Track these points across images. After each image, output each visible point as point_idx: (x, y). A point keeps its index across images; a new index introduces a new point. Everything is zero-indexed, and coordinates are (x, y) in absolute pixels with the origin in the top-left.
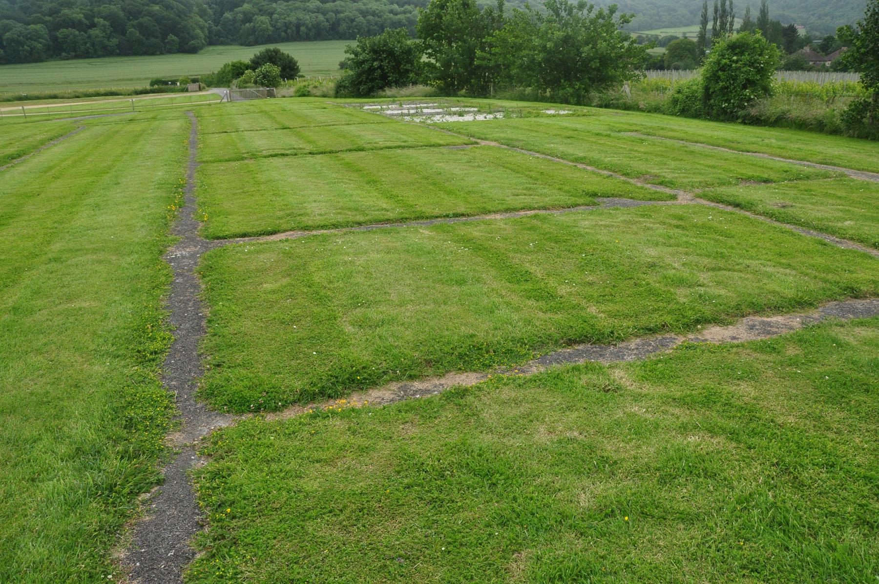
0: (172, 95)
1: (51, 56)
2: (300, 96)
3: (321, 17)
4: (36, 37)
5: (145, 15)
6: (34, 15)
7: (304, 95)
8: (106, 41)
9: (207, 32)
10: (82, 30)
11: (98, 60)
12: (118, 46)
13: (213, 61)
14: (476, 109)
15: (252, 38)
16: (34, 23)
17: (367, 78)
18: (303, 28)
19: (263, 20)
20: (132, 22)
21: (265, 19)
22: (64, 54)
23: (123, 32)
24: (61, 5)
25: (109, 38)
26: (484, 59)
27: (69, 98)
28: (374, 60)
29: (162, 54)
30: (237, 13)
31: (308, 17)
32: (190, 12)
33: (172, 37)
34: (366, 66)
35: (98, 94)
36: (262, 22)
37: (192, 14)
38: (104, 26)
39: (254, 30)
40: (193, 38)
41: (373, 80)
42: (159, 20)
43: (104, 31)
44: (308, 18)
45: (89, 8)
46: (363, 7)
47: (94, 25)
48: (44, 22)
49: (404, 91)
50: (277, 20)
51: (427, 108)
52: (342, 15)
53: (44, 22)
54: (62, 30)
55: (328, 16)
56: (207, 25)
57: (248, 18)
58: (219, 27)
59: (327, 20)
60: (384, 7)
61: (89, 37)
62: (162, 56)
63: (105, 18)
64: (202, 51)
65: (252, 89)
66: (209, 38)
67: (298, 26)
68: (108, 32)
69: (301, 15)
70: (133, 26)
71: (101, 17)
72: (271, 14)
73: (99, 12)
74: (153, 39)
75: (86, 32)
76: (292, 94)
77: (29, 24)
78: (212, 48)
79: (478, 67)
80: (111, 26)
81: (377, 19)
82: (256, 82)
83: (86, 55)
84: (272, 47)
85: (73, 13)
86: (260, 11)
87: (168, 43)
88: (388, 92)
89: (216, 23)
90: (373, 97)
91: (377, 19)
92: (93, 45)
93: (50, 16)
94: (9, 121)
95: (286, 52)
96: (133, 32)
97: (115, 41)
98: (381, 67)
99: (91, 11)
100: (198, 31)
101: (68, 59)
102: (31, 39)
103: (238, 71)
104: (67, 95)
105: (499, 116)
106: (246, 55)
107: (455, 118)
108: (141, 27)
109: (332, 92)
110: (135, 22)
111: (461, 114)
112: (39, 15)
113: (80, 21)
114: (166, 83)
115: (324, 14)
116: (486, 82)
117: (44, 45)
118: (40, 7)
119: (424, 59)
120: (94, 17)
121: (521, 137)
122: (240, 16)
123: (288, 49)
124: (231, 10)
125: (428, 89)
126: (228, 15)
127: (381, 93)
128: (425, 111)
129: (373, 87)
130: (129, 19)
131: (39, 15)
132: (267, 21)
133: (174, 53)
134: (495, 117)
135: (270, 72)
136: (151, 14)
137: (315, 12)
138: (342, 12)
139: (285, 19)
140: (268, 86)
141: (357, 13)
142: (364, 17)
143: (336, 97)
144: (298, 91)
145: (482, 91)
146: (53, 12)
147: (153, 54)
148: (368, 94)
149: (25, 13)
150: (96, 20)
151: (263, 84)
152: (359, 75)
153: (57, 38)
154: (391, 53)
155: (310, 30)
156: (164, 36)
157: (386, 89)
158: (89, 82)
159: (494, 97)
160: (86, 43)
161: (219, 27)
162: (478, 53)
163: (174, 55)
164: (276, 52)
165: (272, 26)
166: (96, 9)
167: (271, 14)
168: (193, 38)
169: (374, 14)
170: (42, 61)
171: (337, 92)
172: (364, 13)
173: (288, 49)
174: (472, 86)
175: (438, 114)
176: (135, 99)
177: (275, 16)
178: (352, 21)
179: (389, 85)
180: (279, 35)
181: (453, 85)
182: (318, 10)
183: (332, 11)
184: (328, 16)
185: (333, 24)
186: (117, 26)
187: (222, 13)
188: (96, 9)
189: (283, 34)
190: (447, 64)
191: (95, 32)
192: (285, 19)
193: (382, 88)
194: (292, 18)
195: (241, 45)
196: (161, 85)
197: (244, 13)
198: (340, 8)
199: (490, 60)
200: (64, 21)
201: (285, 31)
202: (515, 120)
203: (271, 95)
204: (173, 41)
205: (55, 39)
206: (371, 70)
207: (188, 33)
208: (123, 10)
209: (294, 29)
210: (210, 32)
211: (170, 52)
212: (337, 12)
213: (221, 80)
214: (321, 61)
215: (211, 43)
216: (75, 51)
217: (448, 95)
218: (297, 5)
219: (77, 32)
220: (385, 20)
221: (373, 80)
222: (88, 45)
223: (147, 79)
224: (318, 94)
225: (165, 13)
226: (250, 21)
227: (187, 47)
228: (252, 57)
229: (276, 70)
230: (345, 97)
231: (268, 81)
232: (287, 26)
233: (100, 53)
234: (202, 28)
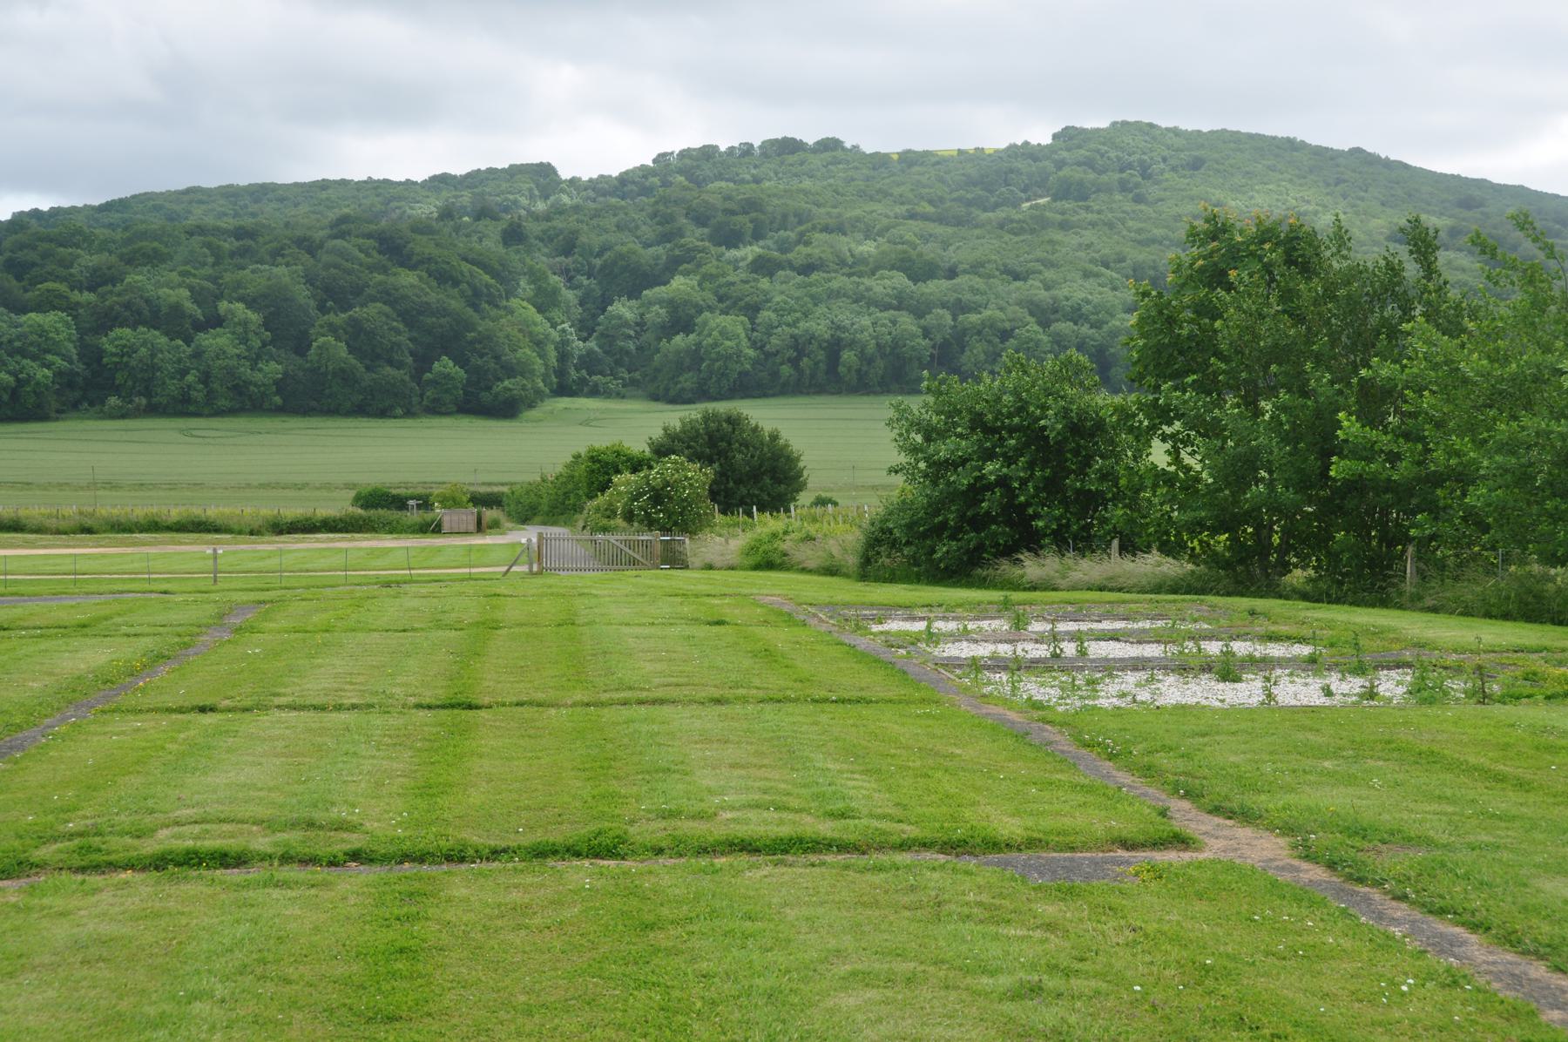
0: (387, 542)
1: (75, 406)
2: (757, 567)
3: (907, 322)
4: (41, 348)
5: (374, 299)
6: (50, 285)
7: (768, 565)
8: (245, 370)
9: (552, 355)
10: (178, 335)
11: (215, 422)
12: (280, 386)
13: (542, 445)
14: (1305, 650)
15: (687, 381)
16: (40, 307)
17: (962, 517)
18: (848, 356)
19: (725, 329)
20: (331, 317)
21: (735, 323)
22: (113, 401)
23: (301, 345)
24: (130, 261)
25: (255, 360)
26: (1366, 452)
27: (58, 532)
28: (989, 455)
29: (409, 414)
30: (651, 303)
31: (866, 321)
32: (510, 294)
33: (445, 365)
34: (963, 480)
35: (154, 526)
36: (724, 333)
37: (514, 302)
38: (245, 323)
39: (695, 356)
40: (510, 371)
41: (979, 523)
42: (410, 315)
43: (244, 340)
44: (865, 325)
45: (208, 271)
46: (1043, 295)
47: (216, 321)
48: (71, 308)
49: (1088, 568)
50: (771, 327)
51: (1114, 637)
52: (974, 318)
53: (71, 308)
54: (118, 331)
55: (929, 320)
56: (555, 335)
57: (681, 319)
58: (592, 344)
59: (926, 332)
60: (1109, 295)
61: (198, 355)
62: (409, 422)
63: (251, 303)
64: (533, 413)
65: (620, 536)
66: (561, 373)
67: (834, 348)
68: (256, 343)
69: (844, 314)
70: (333, 329)
71: (241, 299)
72: (752, 310)
73: (239, 285)
74: (388, 370)
75: (188, 341)
76: (734, 559)
77: (24, 310)
78: (564, 402)
79: (1355, 486)
80: (266, 325)
81: (1085, 329)
82: (629, 516)
83: (181, 407)
84: (722, 407)
85: (159, 285)
86: (721, 299)
87: (430, 382)
88: (1032, 567)
89: (586, 328)
90: (983, 583)
91: (1085, 329)
92: (206, 378)
93: (91, 289)
94: (22, 589)
95: (767, 427)
96: (332, 348)
97: (272, 369)
98: (1003, 482)
99: (214, 280)
100: (527, 352)
101: (123, 417)
102: (23, 353)
103: (601, 470)
104: (52, 523)
105: (1392, 685)
106: (637, 425)
107: (1204, 692)
108: (357, 336)
109: (852, 561)
110: (340, 318)
111: (1228, 671)
112: (62, 287)
113: (176, 309)
114: (400, 503)
115: (919, 312)
116: (1391, 544)
117: (59, 374)
118: (66, 264)
119: (1159, 455)
120: (219, 297)
121: (1425, 818)
122: (658, 314)
123: (766, 416)
124: (634, 294)
125: (1172, 567)
126: (623, 309)
127: (1006, 568)
128: (1098, 650)
129: (980, 547)
130: (322, 309)
131: (62, 287)
132: (740, 330)
133: (447, 414)
134: (1371, 694)
135: (674, 485)
136: (389, 296)
137: (886, 307)
138: (976, 308)
139: (794, 324)
140: (665, 530)
141: (1022, 313)
142: (1045, 324)
143: (864, 577)
144: (752, 549)
145: (1367, 577)
146: (98, 280)
147: (383, 413)
148: (959, 572)
149: (19, 278)
150: (223, 306)
151: (651, 523)
152: (935, 508)
153: (100, 353)
154: (1035, 437)
155: (870, 361)
156: (424, 361)
157: (1025, 556)
158: (173, 486)
159: (1414, 603)
160: (184, 373)
161: (592, 344)
162: (1349, 426)
163: (446, 421)
164: (734, 421)
165: (754, 344)
166: (228, 277)
167: (752, 310)
168: (510, 371)
169: (1076, 315)
170: (44, 418)
171: (867, 561)
172: (1045, 315)
173: (766, 416)
174: (1334, 557)
175: (1137, 665)
176: (269, 545)
177: (766, 315)
178: (1005, 335)
179: (1030, 541)
180: (775, 374)
181: (1263, 548)
182: (900, 302)
183: (944, 306)
184: (929, 320)
185: (944, 346)
186: (284, 328)
187: (605, 302)
188: (228, 277)
189: (786, 370)
190: (1239, 472)
191: (215, 341)
192: (794, 324)
193: (1009, 551)
194: (818, 326)
195: (655, 398)
196: (382, 509)
197: (672, 305)
198: (967, 297)
199: (1393, 458)
200: (127, 306)
201: (794, 362)
202: (1458, 720)
203: (674, 560)
204: (447, 376)
205: (93, 356)
206: (978, 489)
207: (497, 358)
208: (310, 280)
209: (821, 355)
210: (563, 357)
211: (435, 409)
212: (959, 308)
213: (555, 503)
214: (855, 455)
215: (563, 390)
216: (148, 393)
217: (1241, 588)
218: (835, 285)
219: (163, 340)
220: (1114, 334)
221: (979, 523)
222: (190, 378)
223: (348, 486)
224: (811, 564)
225: (433, 296)
226: (687, 326)
227: (488, 398)
228: (657, 434)
229: (698, 476)
230: (892, 579)
231: (669, 514)
232: (800, 347)
233: (223, 403)
234: (539, 344)
